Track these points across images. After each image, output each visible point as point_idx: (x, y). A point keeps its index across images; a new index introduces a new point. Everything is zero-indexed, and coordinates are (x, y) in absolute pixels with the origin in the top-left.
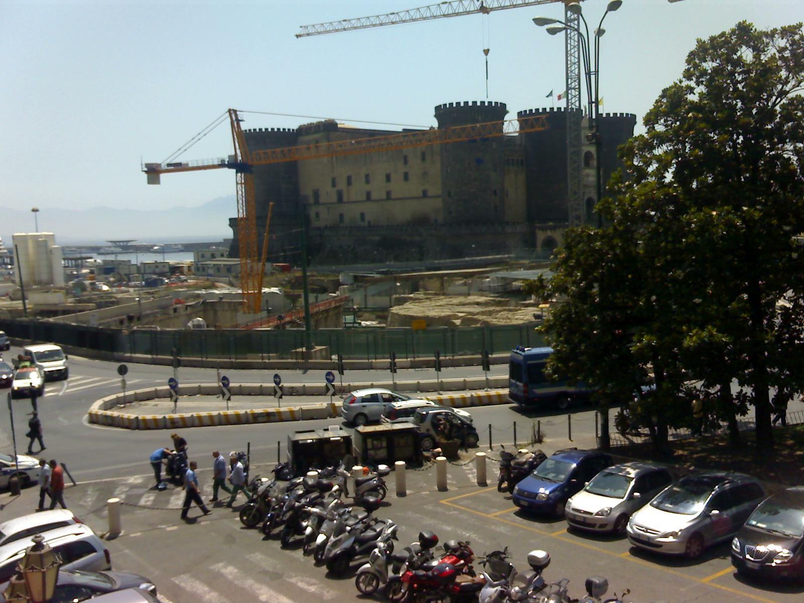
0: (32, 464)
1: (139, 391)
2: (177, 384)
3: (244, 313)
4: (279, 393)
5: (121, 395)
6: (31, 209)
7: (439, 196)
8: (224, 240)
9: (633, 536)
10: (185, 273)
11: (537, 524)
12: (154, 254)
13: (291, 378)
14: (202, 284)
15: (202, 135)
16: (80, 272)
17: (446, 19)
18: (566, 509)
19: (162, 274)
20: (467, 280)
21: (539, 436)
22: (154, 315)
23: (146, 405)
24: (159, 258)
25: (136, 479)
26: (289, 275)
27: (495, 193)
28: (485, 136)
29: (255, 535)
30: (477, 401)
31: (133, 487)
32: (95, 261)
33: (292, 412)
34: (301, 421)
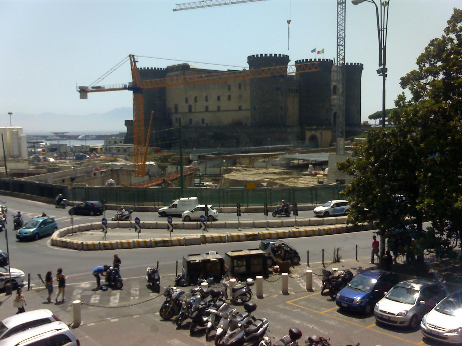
0: (19, 274)
1: (81, 225)
2: (106, 221)
3: (136, 177)
4: (171, 228)
5: (70, 227)
6: (8, 113)
7: (248, 110)
8: (120, 133)
9: (426, 331)
10: (99, 152)
11: (354, 319)
12: (80, 141)
16: (36, 151)
18: (375, 310)
19: (86, 152)
20: (265, 159)
22: (83, 177)
23: (85, 234)
24: (83, 143)
25: (86, 284)
26: (160, 154)
29: (170, 326)
30: (292, 235)
31: (85, 290)
32: (46, 144)
33: (179, 240)
34: (184, 246)
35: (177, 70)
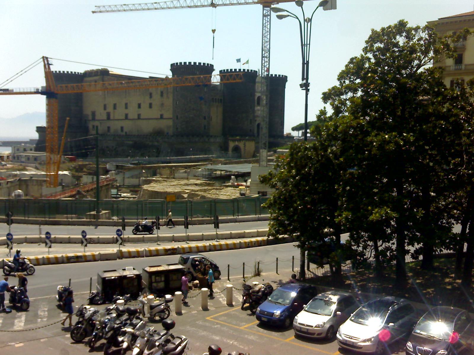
4: (85, 243)
9: (343, 342)
10: (5, 160)
13: (93, 233)
14: (17, 168)
15: (23, 72)
17: (189, 9)
18: (294, 323)
20: (187, 170)
21: (258, 272)
27: (205, 118)
28: (206, 83)
30: (213, 248)
33: (94, 256)
34: (99, 262)
35: (95, 75)
